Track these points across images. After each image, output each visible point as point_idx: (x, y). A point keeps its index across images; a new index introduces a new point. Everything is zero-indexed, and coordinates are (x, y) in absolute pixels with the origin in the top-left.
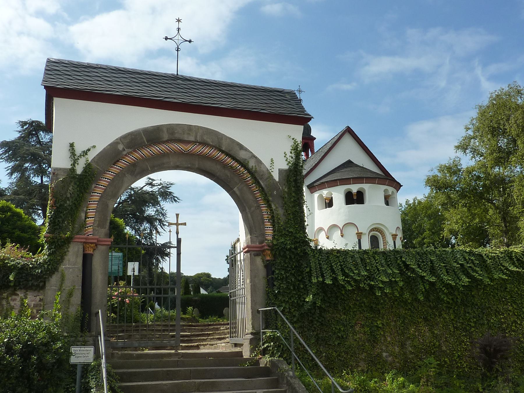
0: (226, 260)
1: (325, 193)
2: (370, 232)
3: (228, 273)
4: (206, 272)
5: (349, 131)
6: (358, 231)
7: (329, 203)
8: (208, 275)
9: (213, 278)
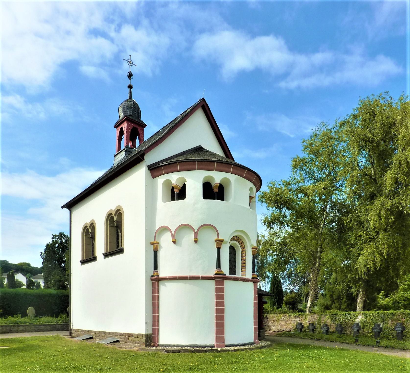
0: (40, 255)
1: (175, 178)
2: (231, 240)
3: (42, 266)
4: (27, 262)
5: (203, 106)
6: (218, 237)
7: (179, 193)
8: (29, 265)
9: (32, 267)
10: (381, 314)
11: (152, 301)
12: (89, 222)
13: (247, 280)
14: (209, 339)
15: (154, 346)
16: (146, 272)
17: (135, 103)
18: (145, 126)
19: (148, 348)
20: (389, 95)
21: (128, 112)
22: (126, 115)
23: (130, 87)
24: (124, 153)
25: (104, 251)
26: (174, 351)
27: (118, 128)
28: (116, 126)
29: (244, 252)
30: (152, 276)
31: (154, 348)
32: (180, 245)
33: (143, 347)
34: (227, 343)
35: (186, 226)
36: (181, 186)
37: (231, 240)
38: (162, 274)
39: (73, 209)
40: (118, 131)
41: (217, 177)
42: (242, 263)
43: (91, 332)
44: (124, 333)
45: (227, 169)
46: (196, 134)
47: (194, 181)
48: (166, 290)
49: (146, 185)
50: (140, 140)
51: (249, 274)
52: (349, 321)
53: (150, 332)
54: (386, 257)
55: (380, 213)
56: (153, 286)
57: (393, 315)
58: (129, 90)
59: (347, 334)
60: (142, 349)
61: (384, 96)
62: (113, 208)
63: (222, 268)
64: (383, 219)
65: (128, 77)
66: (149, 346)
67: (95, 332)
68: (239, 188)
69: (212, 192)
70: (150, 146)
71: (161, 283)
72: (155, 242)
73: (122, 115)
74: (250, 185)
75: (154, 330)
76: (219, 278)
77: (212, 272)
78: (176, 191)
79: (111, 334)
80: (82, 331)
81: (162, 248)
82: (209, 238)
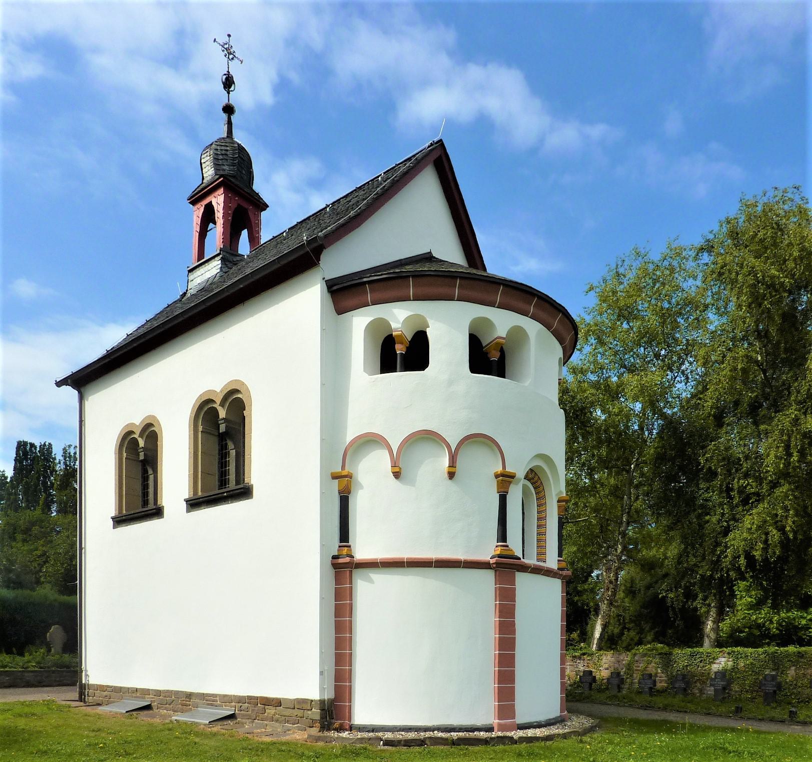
1: (399, 316)
5: (438, 159)
7: (404, 354)
10: (772, 653)
11: (333, 619)
12: (138, 420)
13: (548, 573)
14: (480, 712)
15: (341, 729)
16: (322, 546)
17: (241, 149)
18: (264, 206)
19: (326, 734)
20: (802, 195)
21: (226, 167)
22: (222, 172)
23: (229, 110)
24: (216, 264)
25: (112, 511)
26: (408, 743)
27: (198, 206)
28: (195, 200)
29: (542, 508)
30: (334, 557)
31: (345, 734)
32: (412, 483)
33: (315, 731)
34: (520, 719)
35: (428, 437)
38: (362, 550)
39: (88, 389)
40: (198, 211)
41: (503, 322)
43: (146, 692)
44: (250, 698)
45: (521, 305)
46: (416, 226)
47: (448, 327)
48: (368, 590)
49: (322, 330)
50: (254, 239)
52: (697, 668)
53: (329, 695)
54: (791, 536)
55: (789, 440)
56: (338, 579)
57: (800, 655)
58: (225, 116)
59: (694, 694)
60: (318, 739)
61: (790, 195)
62: (217, 385)
64: (795, 454)
66: (329, 730)
67: (158, 693)
70: (333, 232)
71: (358, 574)
72: (344, 473)
73: (209, 172)
75: (338, 689)
77: (488, 551)
78: (400, 349)
79: (209, 699)
80: (119, 691)
81: (362, 488)
82: (482, 469)
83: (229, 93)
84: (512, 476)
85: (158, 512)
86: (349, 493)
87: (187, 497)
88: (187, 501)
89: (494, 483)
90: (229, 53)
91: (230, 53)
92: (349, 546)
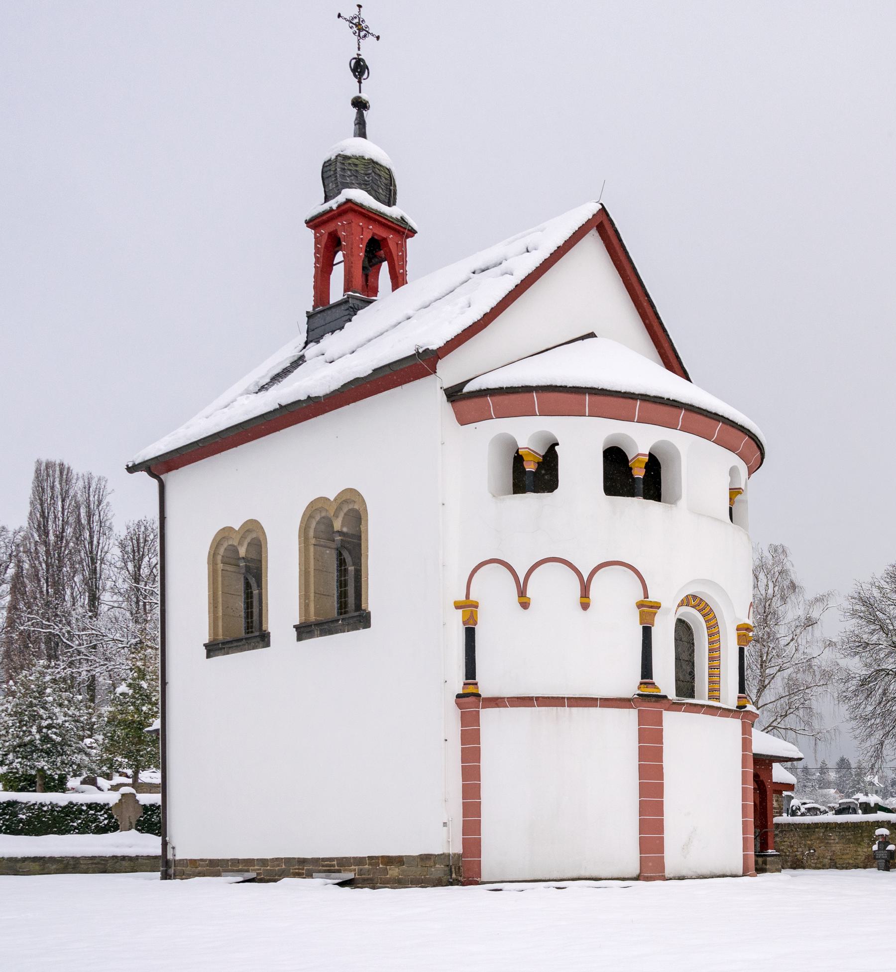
1: (527, 431)
5: (602, 225)
7: (535, 474)
13: (726, 712)
36: (542, 453)
37: (682, 604)
42: (710, 668)
51: (730, 697)
58: (355, 111)
63: (657, 678)
65: (354, 71)
68: (700, 467)
69: (631, 477)
71: (170, 856)
74: (734, 460)
76: (648, 702)
78: (530, 467)
83: (360, 82)
84: (657, 606)
85: (264, 639)
86: (476, 624)
87: (297, 623)
88: (297, 627)
89: (636, 613)
90: (360, 28)
91: (360, 30)
92: (476, 684)
